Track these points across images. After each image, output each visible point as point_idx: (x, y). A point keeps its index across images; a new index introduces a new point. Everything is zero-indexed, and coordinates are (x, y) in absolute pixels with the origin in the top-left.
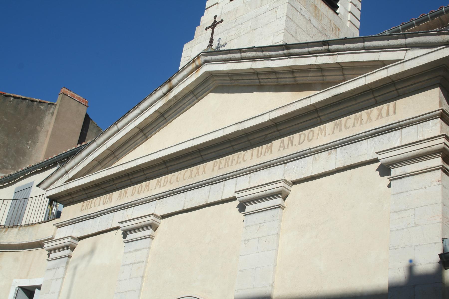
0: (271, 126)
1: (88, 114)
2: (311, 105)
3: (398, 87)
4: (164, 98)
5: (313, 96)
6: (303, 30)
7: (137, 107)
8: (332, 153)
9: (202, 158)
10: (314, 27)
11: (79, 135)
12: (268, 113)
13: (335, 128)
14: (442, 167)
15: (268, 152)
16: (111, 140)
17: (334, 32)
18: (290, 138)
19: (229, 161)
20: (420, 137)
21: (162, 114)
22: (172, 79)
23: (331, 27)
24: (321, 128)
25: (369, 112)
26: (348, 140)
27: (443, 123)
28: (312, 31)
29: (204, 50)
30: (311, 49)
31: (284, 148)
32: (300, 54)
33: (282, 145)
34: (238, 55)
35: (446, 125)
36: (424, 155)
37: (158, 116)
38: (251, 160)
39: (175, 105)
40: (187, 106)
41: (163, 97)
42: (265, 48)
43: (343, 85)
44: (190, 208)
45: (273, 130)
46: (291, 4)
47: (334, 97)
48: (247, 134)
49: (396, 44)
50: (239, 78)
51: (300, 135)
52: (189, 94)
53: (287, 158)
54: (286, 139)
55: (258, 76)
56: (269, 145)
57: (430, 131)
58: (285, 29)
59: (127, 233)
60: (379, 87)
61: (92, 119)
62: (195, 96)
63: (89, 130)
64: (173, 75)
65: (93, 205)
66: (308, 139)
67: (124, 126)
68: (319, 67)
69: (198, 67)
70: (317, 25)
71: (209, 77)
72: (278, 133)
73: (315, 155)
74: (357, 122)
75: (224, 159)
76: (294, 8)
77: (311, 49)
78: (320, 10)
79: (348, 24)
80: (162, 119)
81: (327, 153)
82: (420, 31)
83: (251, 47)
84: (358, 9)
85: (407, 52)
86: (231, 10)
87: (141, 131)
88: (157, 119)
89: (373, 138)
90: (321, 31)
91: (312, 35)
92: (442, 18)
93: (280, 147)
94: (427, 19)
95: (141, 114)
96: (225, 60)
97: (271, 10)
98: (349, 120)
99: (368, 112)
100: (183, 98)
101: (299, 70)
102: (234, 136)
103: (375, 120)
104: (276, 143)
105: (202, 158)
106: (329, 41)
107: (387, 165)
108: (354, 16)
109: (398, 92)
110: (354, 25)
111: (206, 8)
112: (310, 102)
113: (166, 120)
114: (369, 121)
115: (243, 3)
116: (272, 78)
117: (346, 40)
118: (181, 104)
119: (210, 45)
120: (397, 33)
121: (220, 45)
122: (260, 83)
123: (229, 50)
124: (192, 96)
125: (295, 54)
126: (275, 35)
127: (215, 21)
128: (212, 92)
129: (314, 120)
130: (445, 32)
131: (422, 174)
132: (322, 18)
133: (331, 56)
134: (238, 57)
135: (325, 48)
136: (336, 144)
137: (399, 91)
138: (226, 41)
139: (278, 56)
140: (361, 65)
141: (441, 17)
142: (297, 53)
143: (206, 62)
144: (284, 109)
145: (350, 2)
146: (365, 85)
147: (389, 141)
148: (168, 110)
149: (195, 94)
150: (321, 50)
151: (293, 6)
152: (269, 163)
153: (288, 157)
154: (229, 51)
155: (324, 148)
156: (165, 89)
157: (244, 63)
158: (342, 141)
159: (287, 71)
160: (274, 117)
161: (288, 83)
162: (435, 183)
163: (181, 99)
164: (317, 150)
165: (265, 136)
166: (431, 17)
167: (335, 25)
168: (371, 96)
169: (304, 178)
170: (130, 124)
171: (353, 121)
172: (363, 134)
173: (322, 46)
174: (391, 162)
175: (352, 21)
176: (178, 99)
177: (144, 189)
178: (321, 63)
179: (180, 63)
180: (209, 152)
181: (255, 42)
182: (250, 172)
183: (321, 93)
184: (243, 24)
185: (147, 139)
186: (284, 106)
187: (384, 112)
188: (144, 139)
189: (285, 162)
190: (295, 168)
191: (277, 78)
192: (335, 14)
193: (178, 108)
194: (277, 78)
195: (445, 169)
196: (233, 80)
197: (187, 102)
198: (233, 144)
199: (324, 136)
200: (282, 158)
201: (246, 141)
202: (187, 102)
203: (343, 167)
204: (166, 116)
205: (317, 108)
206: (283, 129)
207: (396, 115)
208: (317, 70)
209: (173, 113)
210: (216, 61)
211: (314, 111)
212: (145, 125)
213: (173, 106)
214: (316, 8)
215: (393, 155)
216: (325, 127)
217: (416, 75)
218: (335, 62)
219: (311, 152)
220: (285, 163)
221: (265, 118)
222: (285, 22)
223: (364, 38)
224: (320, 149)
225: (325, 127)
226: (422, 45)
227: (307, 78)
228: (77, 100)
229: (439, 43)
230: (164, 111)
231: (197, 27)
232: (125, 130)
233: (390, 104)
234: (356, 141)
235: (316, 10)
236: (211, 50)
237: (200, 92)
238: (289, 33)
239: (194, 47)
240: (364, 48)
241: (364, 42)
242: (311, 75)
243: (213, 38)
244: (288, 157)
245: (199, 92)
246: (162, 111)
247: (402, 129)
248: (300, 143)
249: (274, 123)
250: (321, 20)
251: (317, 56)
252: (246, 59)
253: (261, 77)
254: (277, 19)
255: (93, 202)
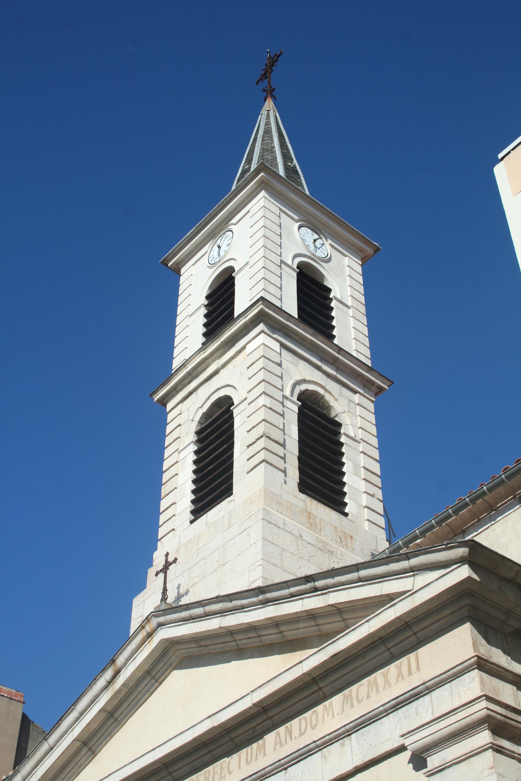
0: (258, 713)
1: (27, 714)
2: (303, 674)
3: (415, 629)
4: (109, 688)
5: (305, 659)
6: (292, 553)
7: (73, 709)
8: (345, 744)
9: (172, 776)
10: (309, 545)
11: (15, 751)
12: (249, 694)
13: (344, 703)
14: (491, 746)
15: (260, 754)
16: (41, 766)
17: (343, 544)
18: (287, 727)
19: (209, 775)
20: (456, 701)
21: (110, 714)
22: (117, 658)
23: (338, 538)
24: (326, 707)
25: (385, 672)
26: (364, 721)
27: (484, 675)
28: (307, 551)
29: (155, 608)
30: (293, 590)
31: (281, 745)
32: (280, 598)
33: (278, 741)
34: (199, 611)
35: (489, 676)
36: (464, 730)
37: (106, 717)
38: (238, 769)
39: (127, 696)
40: (144, 695)
41: (107, 687)
42: (233, 596)
43: (341, 639)
44: (347, 772)
45: (261, 719)
46: (267, 521)
47: (333, 658)
48: (227, 729)
49: (399, 569)
50: (209, 642)
51: (300, 720)
52: (144, 676)
53: (286, 761)
54: (282, 729)
55: (232, 637)
56: (261, 742)
57: (467, 691)
58: (262, 559)
59: (425, 755)
60: (390, 633)
61: (33, 721)
62: (153, 677)
63: (30, 739)
64: (117, 652)
65: (225, 772)
66: (311, 726)
67: (58, 741)
68: (308, 614)
69: (150, 635)
70: (313, 541)
71: (169, 646)
72: (269, 721)
73: (323, 750)
74: (372, 690)
75: (202, 774)
76: (273, 524)
77: (293, 590)
78: (316, 516)
79: (366, 525)
80: (112, 720)
81: (339, 744)
82: (424, 548)
83: (214, 596)
84: (378, 499)
85: (416, 577)
86: (192, 538)
87: (83, 744)
88: (104, 723)
89: (396, 712)
90: (322, 547)
91: (308, 558)
92: (487, 499)
93: (276, 744)
94: (467, 505)
95: (80, 717)
96: (185, 619)
97: (241, 533)
98: (361, 687)
99: (384, 672)
100: (136, 684)
101: (284, 621)
102: (210, 737)
103: (395, 684)
104: (270, 738)
105: (172, 776)
106: (313, 576)
107: (419, 753)
108: (373, 510)
109: (417, 637)
110: (375, 524)
111: (159, 538)
112: (302, 671)
113: (118, 721)
114: (387, 686)
115: (206, 526)
116: (253, 637)
117: (334, 571)
118: (135, 694)
119: (164, 598)
120: (396, 554)
121: (181, 594)
122: (238, 646)
123: (187, 605)
124: (149, 679)
125: (274, 600)
126: (251, 570)
127: (166, 560)
128: (176, 668)
129: (314, 695)
130: (455, 544)
131: (467, 761)
132: (321, 527)
133: (321, 597)
134: (201, 613)
135: (310, 586)
136: (349, 729)
137: (418, 634)
138: (188, 587)
139: (252, 605)
140: (364, 602)
141: (485, 498)
142: (276, 598)
143: (160, 625)
144: (270, 686)
145: (364, 492)
146: (370, 634)
147: (418, 713)
148: (118, 705)
149: (153, 675)
150: (305, 590)
151: (271, 522)
152: (262, 772)
153: (287, 759)
154: (187, 606)
155: (333, 737)
156: (108, 674)
157: (211, 620)
158: (355, 723)
159: (269, 625)
160: (258, 700)
161: (275, 641)
162: (487, 772)
163: (135, 686)
164: (325, 742)
165: (253, 730)
166: (471, 501)
167: (345, 533)
168: (383, 648)
169: (369, 761)
170: (66, 737)
171: (367, 689)
172: (382, 708)
173: (306, 584)
174: (423, 747)
175: (371, 520)
176: (130, 686)
177: (255, 753)
178: (309, 608)
179: (130, 629)
180: (180, 765)
181: (226, 583)
182: (318, 749)
183: (315, 654)
184: (208, 557)
185: (95, 756)
186: (269, 681)
187: (405, 670)
188: (90, 756)
189: (284, 767)
190: (300, 775)
191: (259, 636)
192: (342, 517)
193: (133, 700)
194: (259, 636)
195: (497, 747)
196: (201, 646)
197: (143, 688)
198: (211, 748)
199: (332, 718)
200: (279, 762)
201: (228, 742)
202: (143, 688)
203: (362, 764)
204: (116, 716)
205: (315, 676)
206: (275, 715)
207: (420, 671)
208: (308, 618)
209: (125, 709)
210: (172, 622)
211: (312, 681)
212: (88, 734)
213: (124, 699)
214: (309, 515)
215: (424, 736)
216: (331, 703)
217: (435, 609)
218: (327, 605)
219: (317, 747)
220: (286, 769)
221: (246, 704)
222: (261, 548)
223: (357, 566)
224: (328, 740)
225: (331, 702)
226: (432, 566)
227: (298, 631)
228: (5, 695)
229: (451, 560)
230: (112, 707)
231: (149, 570)
232: (60, 747)
233: (410, 656)
234: (374, 719)
235: (309, 518)
236: (165, 606)
237: (160, 670)
238: (271, 563)
239: (146, 601)
240: (360, 580)
241: (358, 571)
242: (303, 626)
243: (166, 587)
244: (287, 759)
245: (158, 672)
246: (109, 709)
247: (432, 693)
248: (301, 734)
249: (260, 708)
250: (320, 531)
251: (302, 599)
252: (211, 614)
253: (238, 637)
254: (250, 546)
255: (225, 765)
